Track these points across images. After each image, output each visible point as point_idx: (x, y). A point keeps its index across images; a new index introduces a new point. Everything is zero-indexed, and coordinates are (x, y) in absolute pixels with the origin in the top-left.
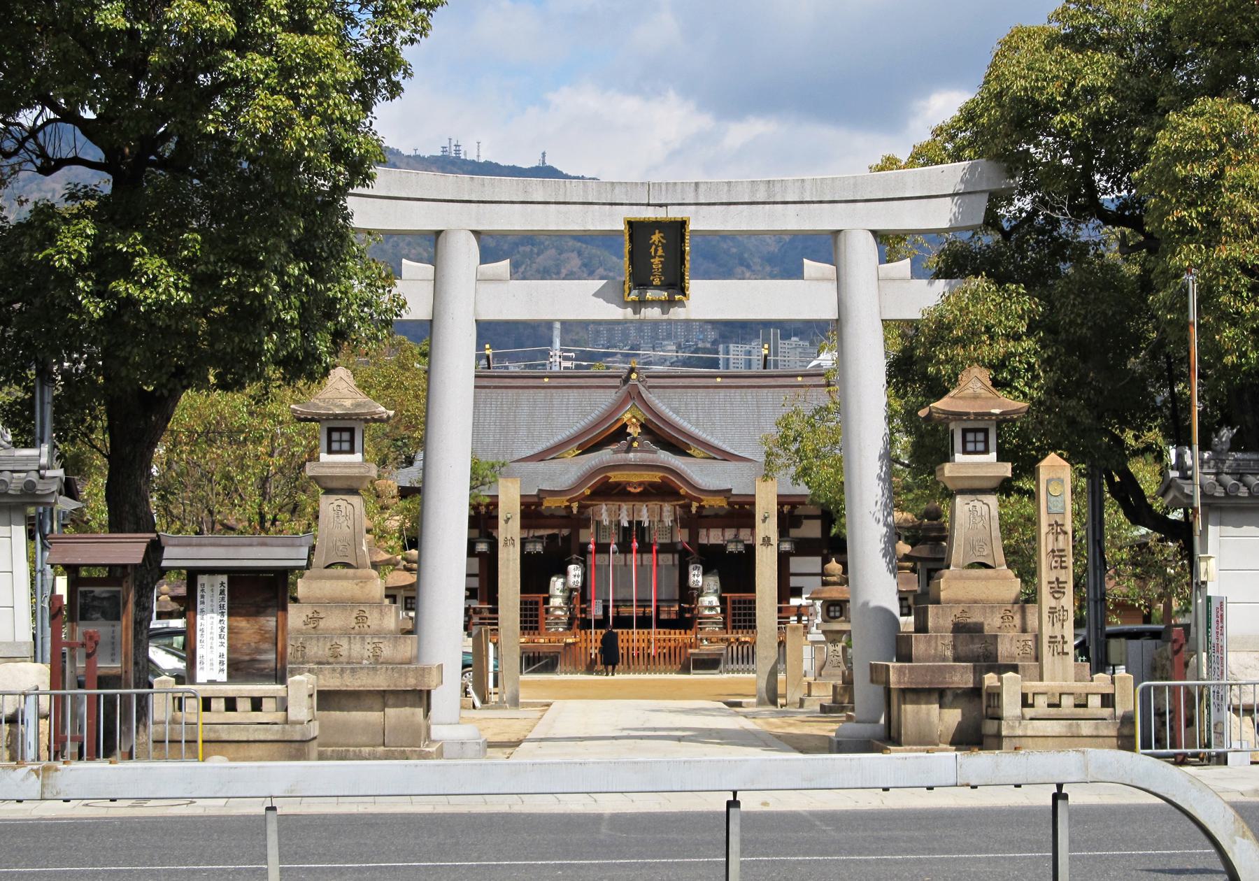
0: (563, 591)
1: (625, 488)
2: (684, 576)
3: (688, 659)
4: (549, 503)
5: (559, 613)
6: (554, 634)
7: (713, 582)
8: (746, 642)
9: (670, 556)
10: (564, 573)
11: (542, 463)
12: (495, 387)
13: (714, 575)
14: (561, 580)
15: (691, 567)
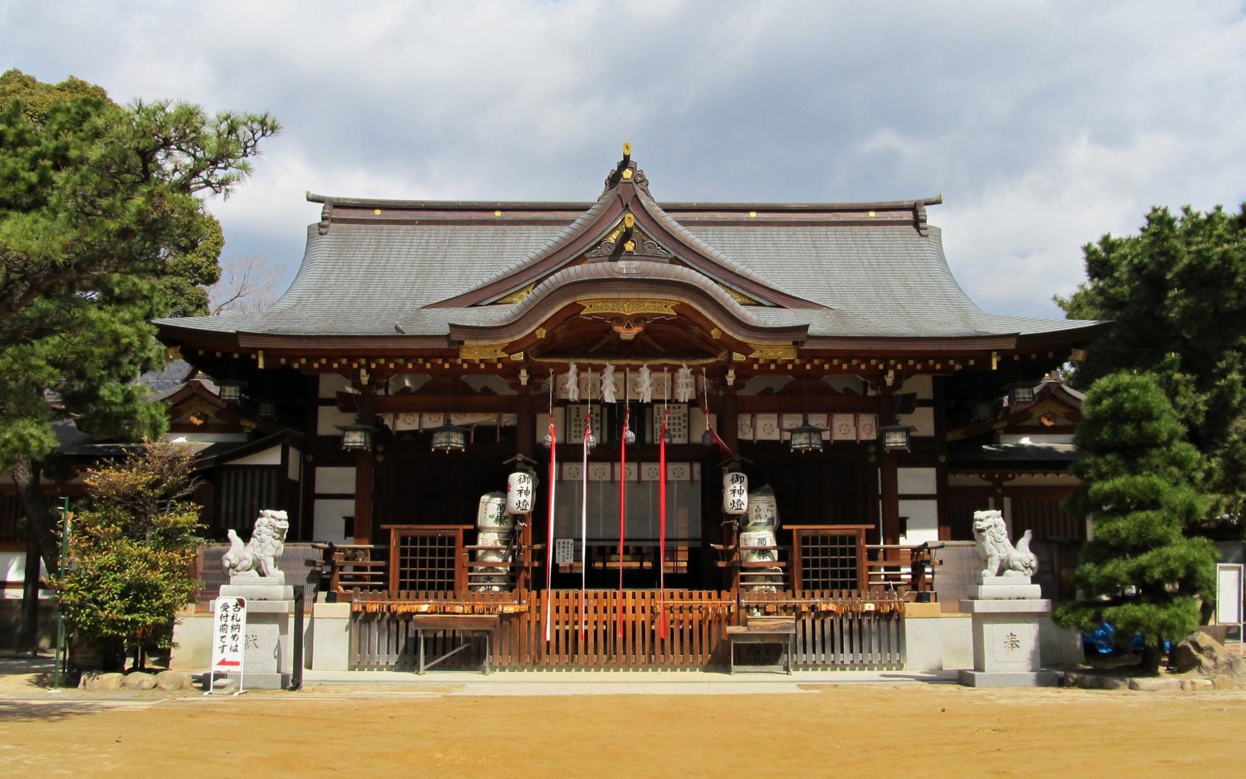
0: (501, 519)
1: (608, 330)
2: (713, 493)
3: (725, 644)
4: (473, 352)
5: (493, 558)
6: (482, 597)
7: (765, 507)
8: (828, 613)
9: (686, 467)
10: (502, 488)
11: (475, 309)
12: (422, 222)
13: (765, 493)
14: (498, 500)
15: (728, 478)
